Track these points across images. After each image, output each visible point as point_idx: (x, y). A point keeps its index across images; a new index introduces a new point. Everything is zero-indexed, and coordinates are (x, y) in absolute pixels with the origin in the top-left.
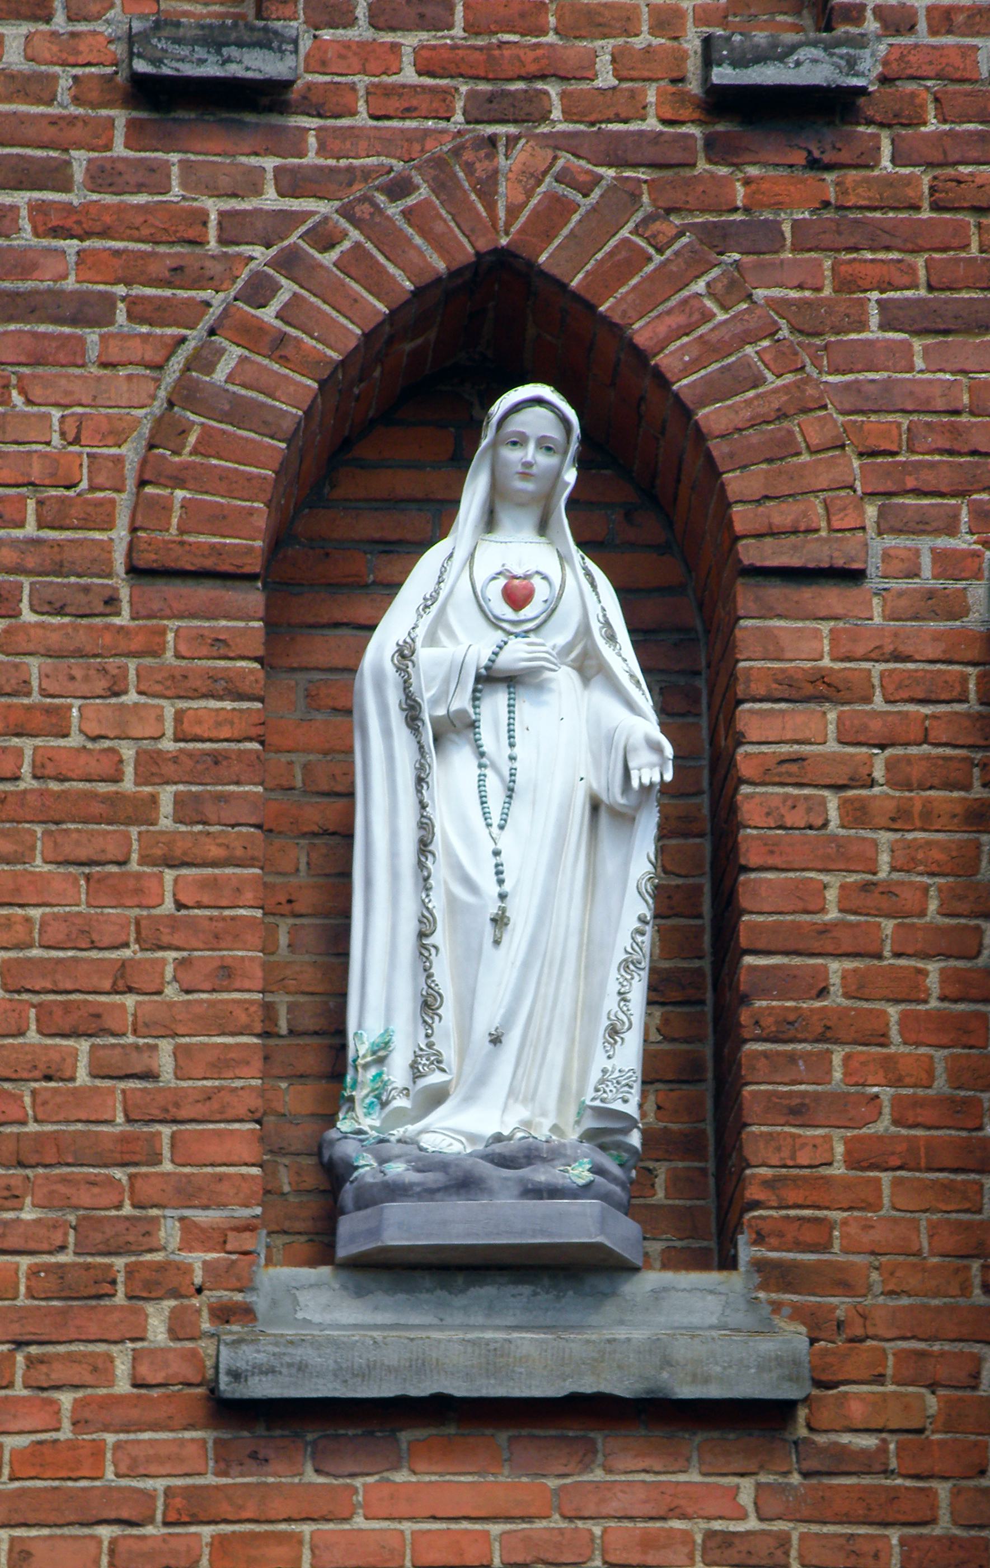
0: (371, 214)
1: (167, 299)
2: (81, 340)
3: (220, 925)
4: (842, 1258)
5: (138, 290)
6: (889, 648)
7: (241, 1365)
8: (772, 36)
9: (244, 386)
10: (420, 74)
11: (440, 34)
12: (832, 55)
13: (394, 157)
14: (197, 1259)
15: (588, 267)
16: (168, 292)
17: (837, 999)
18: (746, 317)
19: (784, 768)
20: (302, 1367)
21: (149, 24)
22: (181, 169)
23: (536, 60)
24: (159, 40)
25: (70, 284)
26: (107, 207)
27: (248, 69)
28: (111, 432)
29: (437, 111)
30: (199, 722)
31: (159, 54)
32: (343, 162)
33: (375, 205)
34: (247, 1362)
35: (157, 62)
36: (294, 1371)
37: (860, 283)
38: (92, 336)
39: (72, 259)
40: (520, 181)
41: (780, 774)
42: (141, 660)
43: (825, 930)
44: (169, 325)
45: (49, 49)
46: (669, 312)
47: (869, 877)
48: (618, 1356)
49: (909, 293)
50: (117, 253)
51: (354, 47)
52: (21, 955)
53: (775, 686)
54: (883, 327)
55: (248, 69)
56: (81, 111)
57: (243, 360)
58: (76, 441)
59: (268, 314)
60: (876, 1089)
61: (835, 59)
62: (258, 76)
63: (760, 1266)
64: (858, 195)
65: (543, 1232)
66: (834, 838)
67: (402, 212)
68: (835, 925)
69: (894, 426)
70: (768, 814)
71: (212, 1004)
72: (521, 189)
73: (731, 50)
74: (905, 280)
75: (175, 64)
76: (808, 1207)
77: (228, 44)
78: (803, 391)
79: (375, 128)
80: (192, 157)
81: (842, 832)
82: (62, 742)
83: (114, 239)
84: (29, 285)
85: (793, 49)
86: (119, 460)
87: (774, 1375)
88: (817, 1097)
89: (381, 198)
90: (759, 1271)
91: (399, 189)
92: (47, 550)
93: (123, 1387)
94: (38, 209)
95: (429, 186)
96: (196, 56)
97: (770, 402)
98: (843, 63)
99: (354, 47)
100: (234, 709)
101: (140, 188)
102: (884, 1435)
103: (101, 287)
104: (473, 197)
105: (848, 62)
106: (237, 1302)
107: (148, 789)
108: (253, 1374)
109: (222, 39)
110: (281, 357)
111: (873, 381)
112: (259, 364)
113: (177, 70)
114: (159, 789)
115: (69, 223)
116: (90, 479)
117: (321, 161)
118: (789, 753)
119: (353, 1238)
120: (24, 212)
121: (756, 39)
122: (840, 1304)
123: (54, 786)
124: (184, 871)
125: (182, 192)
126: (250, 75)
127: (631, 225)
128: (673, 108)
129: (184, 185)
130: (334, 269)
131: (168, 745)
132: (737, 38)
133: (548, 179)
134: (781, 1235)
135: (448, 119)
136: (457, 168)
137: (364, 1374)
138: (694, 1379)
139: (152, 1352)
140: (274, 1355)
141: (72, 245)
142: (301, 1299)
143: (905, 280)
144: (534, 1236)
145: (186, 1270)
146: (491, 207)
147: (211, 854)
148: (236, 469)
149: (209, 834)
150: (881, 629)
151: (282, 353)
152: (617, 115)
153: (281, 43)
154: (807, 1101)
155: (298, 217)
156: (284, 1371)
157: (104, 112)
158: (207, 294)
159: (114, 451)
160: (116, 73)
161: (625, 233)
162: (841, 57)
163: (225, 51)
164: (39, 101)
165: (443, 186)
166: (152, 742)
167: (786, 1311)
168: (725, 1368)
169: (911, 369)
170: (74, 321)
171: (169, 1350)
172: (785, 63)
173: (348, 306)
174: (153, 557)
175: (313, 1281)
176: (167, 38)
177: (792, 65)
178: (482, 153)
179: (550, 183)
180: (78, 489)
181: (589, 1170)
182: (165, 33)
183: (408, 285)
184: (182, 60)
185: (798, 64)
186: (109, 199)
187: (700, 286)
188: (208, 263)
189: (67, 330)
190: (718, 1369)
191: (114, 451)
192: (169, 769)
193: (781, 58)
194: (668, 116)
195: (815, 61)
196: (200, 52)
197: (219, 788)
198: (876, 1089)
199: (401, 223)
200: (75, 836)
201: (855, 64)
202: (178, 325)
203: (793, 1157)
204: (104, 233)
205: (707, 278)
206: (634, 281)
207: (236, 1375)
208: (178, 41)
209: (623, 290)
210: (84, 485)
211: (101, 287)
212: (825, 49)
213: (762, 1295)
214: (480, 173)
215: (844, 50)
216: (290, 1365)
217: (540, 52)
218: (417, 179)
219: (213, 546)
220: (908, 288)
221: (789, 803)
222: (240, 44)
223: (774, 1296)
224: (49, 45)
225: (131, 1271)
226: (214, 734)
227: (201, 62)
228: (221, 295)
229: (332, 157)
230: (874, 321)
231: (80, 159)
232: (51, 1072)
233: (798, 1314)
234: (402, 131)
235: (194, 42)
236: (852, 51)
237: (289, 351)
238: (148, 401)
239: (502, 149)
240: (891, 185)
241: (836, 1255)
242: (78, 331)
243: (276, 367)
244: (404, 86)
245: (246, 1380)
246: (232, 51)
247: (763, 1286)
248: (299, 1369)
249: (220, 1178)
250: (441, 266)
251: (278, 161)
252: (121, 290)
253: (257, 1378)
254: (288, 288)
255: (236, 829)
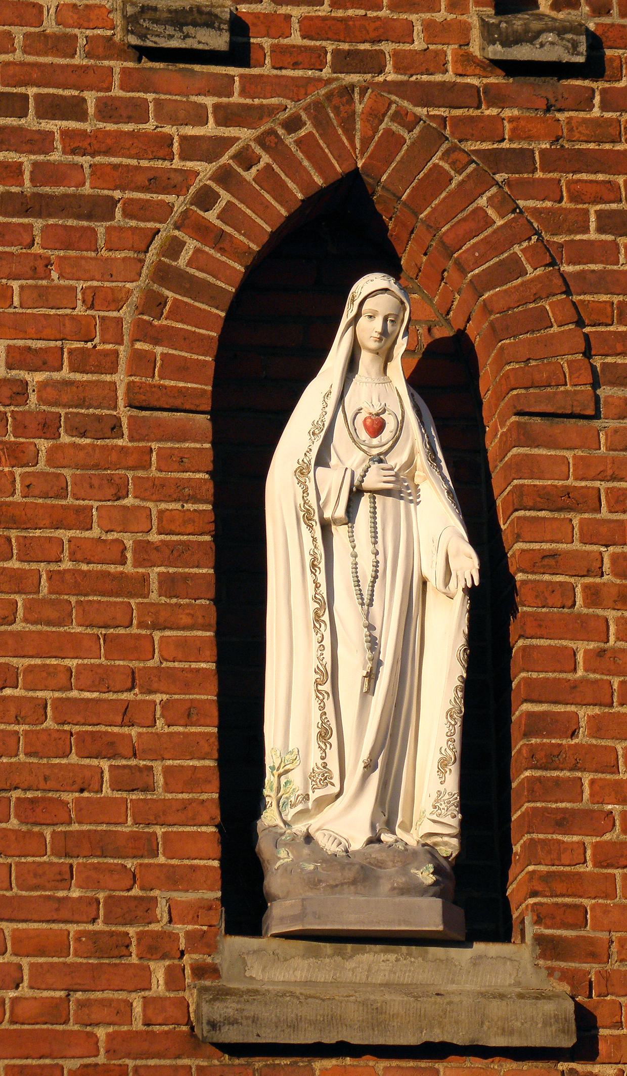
0: (276, 144)
1: (148, 201)
2: (94, 231)
3: (189, 675)
4: (592, 934)
5: (129, 195)
6: (609, 472)
7: (217, 1017)
8: (525, 24)
9: (198, 269)
10: (303, 37)
11: (315, 8)
12: (562, 39)
13: (288, 98)
14: (180, 929)
15: (414, 184)
16: (148, 196)
17: (583, 738)
18: (513, 224)
19: (546, 561)
20: (255, 1020)
21: (138, 9)
22: (155, 106)
23: (376, 29)
24: (144, 21)
25: (87, 190)
26: (108, 133)
27: (199, 42)
28: (114, 301)
29: (314, 65)
30: (172, 520)
31: (144, 31)
32: (257, 101)
33: (277, 136)
34: (220, 1015)
35: (143, 37)
36: (250, 1022)
37: (583, 197)
38: (101, 228)
39: (87, 171)
40: (370, 120)
41: (544, 566)
42: (136, 472)
43: (574, 686)
44: (149, 221)
45: (72, 17)
46: (463, 220)
47: (602, 645)
48: (455, 1014)
49: (614, 206)
50: (115, 167)
51: (262, 18)
52: (64, 695)
53: (538, 499)
54: (600, 230)
55: (199, 42)
56: (92, 62)
57: (197, 251)
58: (92, 307)
59: (212, 216)
60: (610, 807)
61: (565, 42)
62: (207, 48)
63: (539, 940)
64: (580, 132)
65: (406, 922)
66: (580, 615)
67: (295, 141)
68: (583, 680)
69: (608, 305)
70: (537, 597)
71: (186, 735)
72: (369, 127)
73: (500, 34)
74: (612, 197)
75: (154, 39)
76: (569, 896)
77: (187, 24)
78: (551, 281)
79: (277, 76)
80: (163, 97)
81: (585, 611)
82: (87, 534)
83: (114, 156)
84: (62, 190)
85: (539, 34)
86: (119, 321)
87: (554, 1028)
88: (573, 812)
89: (281, 131)
90: (539, 944)
91: (293, 125)
92: (74, 389)
93: (138, 1025)
94: (66, 134)
95: (312, 123)
96: (167, 32)
97: (530, 289)
98: (570, 45)
99: (262, 18)
100: (195, 510)
101: (129, 120)
102: (620, 1066)
103: (106, 192)
104: (340, 132)
105: (573, 45)
106: (208, 964)
107: (141, 570)
108: (224, 1024)
109: (182, 21)
110: (221, 249)
111: (593, 271)
112: (207, 253)
113: (155, 43)
114: (149, 570)
115: (85, 144)
116: (102, 336)
117: (242, 100)
118: (550, 550)
119: (282, 920)
120: (57, 136)
121: (515, 26)
122: (593, 969)
123: (84, 567)
124: (168, 633)
125: (155, 123)
126: (201, 47)
127: (439, 154)
128: (462, 65)
129: (157, 118)
130: (253, 183)
131: (154, 537)
132: (504, 25)
133: (386, 119)
134: (553, 917)
135: (321, 70)
136: (329, 109)
137: (294, 1026)
138: (503, 1032)
139: (154, 999)
140: (237, 1010)
141: (85, 161)
142: (249, 962)
143: (612, 197)
144: (400, 925)
145: (174, 937)
146: (351, 140)
147: (183, 621)
148: (194, 332)
149: (181, 605)
150: (603, 458)
151: (222, 246)
152: (427, 70)
153: (220, 23)
154: (567, 816)
155: (230, 141)
156: (244, 1022)
157: (106, 63)
158: (170, 198)
159: (115, 314)
160: (114, 35)
161: (435, 160)
162: (568, 41)
163: (185, 29)
164: (65, 56)
165: (321, 122)
166: (145, 535)
167: (557, 974)
168: (522, 1024)
169: (617, 263)
170: (89, 217)
171: (166, 998)
172: (534, 45)
173: (264, 209)
174: (144, 398)
175: (256, 948)
176: (149, 19)
177: (538, 46)
178: (344, 99)
179: (388, 122)
180: (94, 343)
181: (433, 873)
182: (147, 16)
183: (300, 196)
184: (158, 36)
185: (542, 45)
186: (110, 127)
187: (482, 201)
188: (172, 175)
189: (85, 223)
190: (519, 1024)
191: (115, 314)
192: (154, 556)
193: (531, 41)
194: (460, 72)
195: (552, 43)
196: (170, 30)
197: (187, 570)
198: (610, 807)
199: (293, 148)
200: (96, 605)
201: (577, 46)
202: (155, 221)
203: (559, 859)
204: (107, 152)
205: (488, 194)
206: (442, 196)
207: (213, 1025)
208: (156, 21)
209: (436, 202)
210: (97, 340)
211: (106, 192)
212: (559, 35)
213: (541, 962)
214: (343, 115)
215: (569, 36)
216: (247, 1018)
217: (378, 23)
218: (304, 117)
219: (180, 389)
220: (613, 202)
221: (550, 588)
222: (195, 24)
223: (549, 963)
224: (71, 14)
225: (141, 936)
226: (182, 530)
227: (171, 37)
228: (181, 198)
229: (249, 97)
230: (593, 225)
231: (91, 98)
232: (85, 786)
233: (565, 976)
234: (293, 78)
235: (166, 22)
236: (575, 37)
237: (226, 244)
238: (137, 277)
239: (356, 96)
240: (600, 125)
241: (588, 932)
242: (92, 224)
243: (218, 255)
244: (294, 46)
245: (220, 1029)
246: (189, 29)
247: (543, 956)
248: (253, 1021)
249: (194, 868)
250: (319, 181)
251: (216, 100)
252: (117, 194)
253: (227, 1027)
254: (225, 197)
255: (198, 602)
